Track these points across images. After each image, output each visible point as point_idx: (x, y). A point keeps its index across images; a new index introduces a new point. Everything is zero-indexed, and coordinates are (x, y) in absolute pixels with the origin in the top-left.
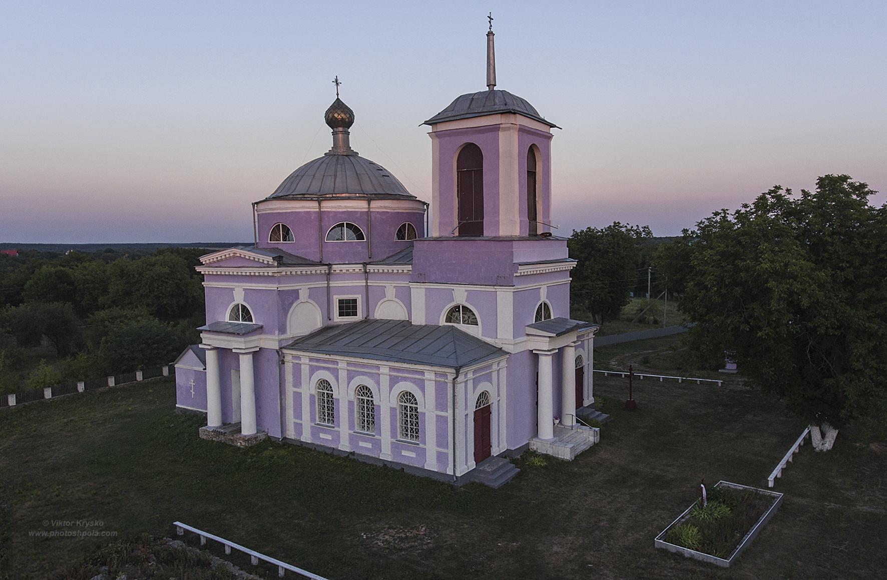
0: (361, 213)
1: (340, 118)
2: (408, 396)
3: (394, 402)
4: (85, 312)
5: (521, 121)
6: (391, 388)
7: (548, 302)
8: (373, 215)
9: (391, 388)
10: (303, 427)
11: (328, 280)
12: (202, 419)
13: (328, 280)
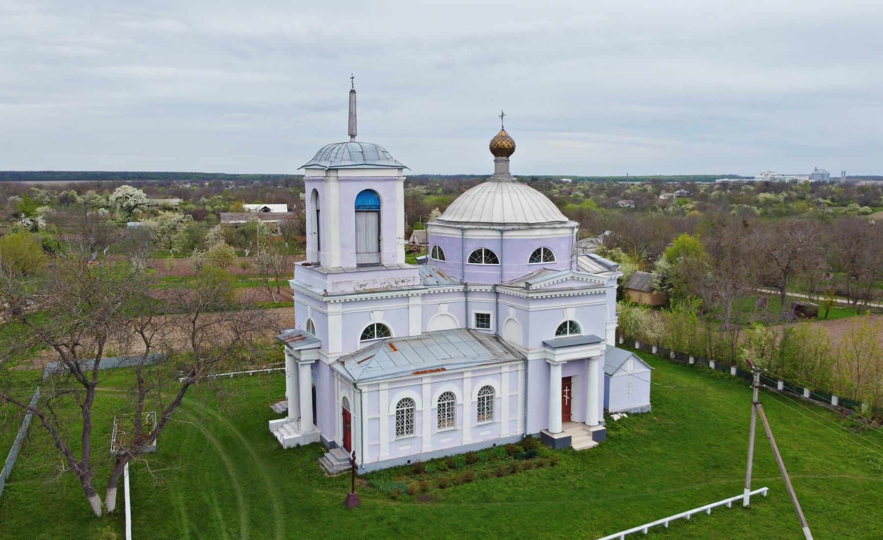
13: (466, 296)
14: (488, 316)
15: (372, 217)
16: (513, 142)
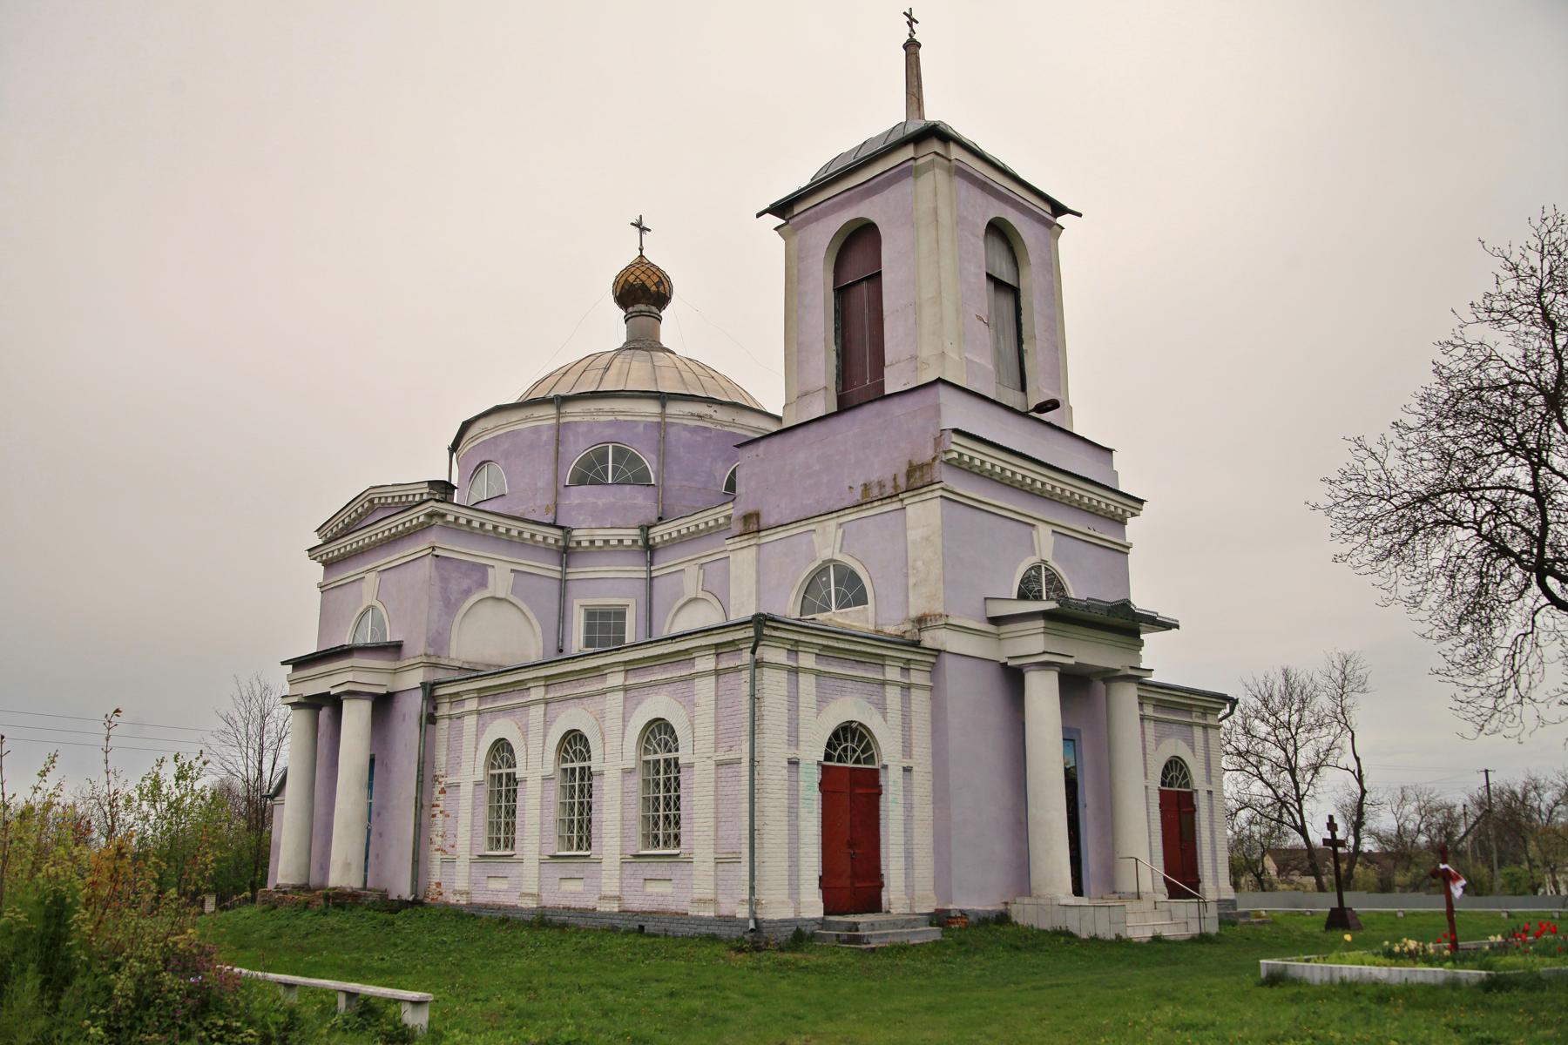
0: (647, 425)
1: (642, 293)
5: (955, 152)
8: (672, 431)
10: (460, 878)
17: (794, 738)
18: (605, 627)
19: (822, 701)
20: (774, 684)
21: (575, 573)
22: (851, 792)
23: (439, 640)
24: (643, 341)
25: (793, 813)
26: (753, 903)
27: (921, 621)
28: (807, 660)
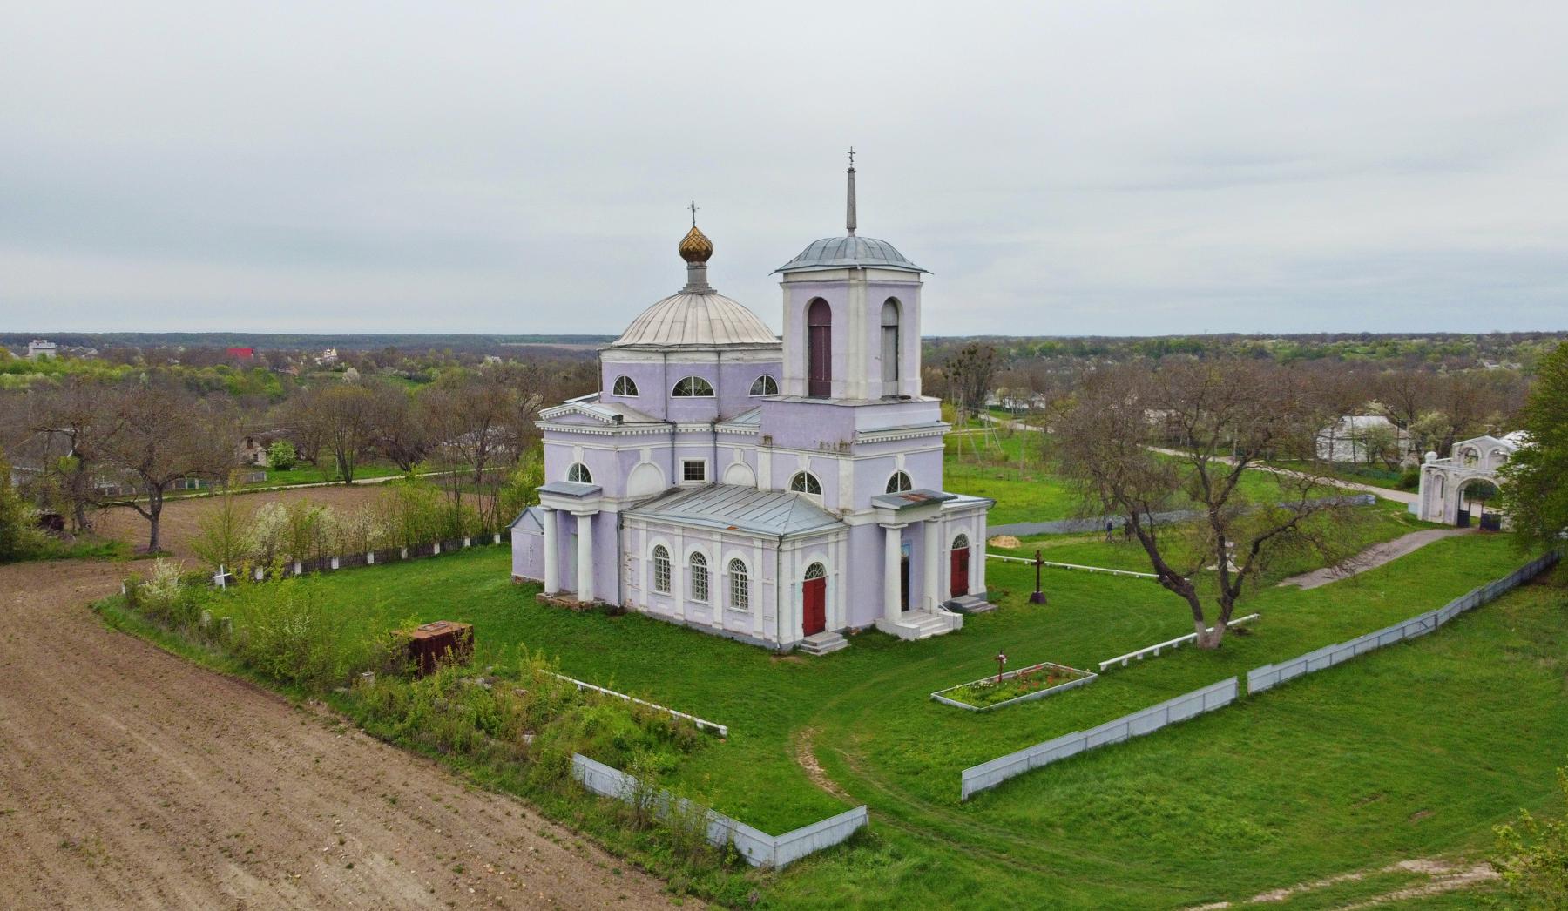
2: (737, 564)
3: (725, 570)
4: (299, 512)
6: (722, 555)
7: (906, 471)
9: (722, 555)
10: (642, 597)
11: (673, 440)
12: (541, 587)
13: (673, 440)
14: (702, 464)
15: (891, 334)
16: (709, 242)
17: (793, 576)
18: (693, 471)
19: (804, 558)
20: (786, 558)
21: (678, 444)
22: (814, 591)
23: (622, 490)
24: (698, 288)
25: (793, 603)
26: (778, 637)
27: (843, 511)
28: (798, 545)
